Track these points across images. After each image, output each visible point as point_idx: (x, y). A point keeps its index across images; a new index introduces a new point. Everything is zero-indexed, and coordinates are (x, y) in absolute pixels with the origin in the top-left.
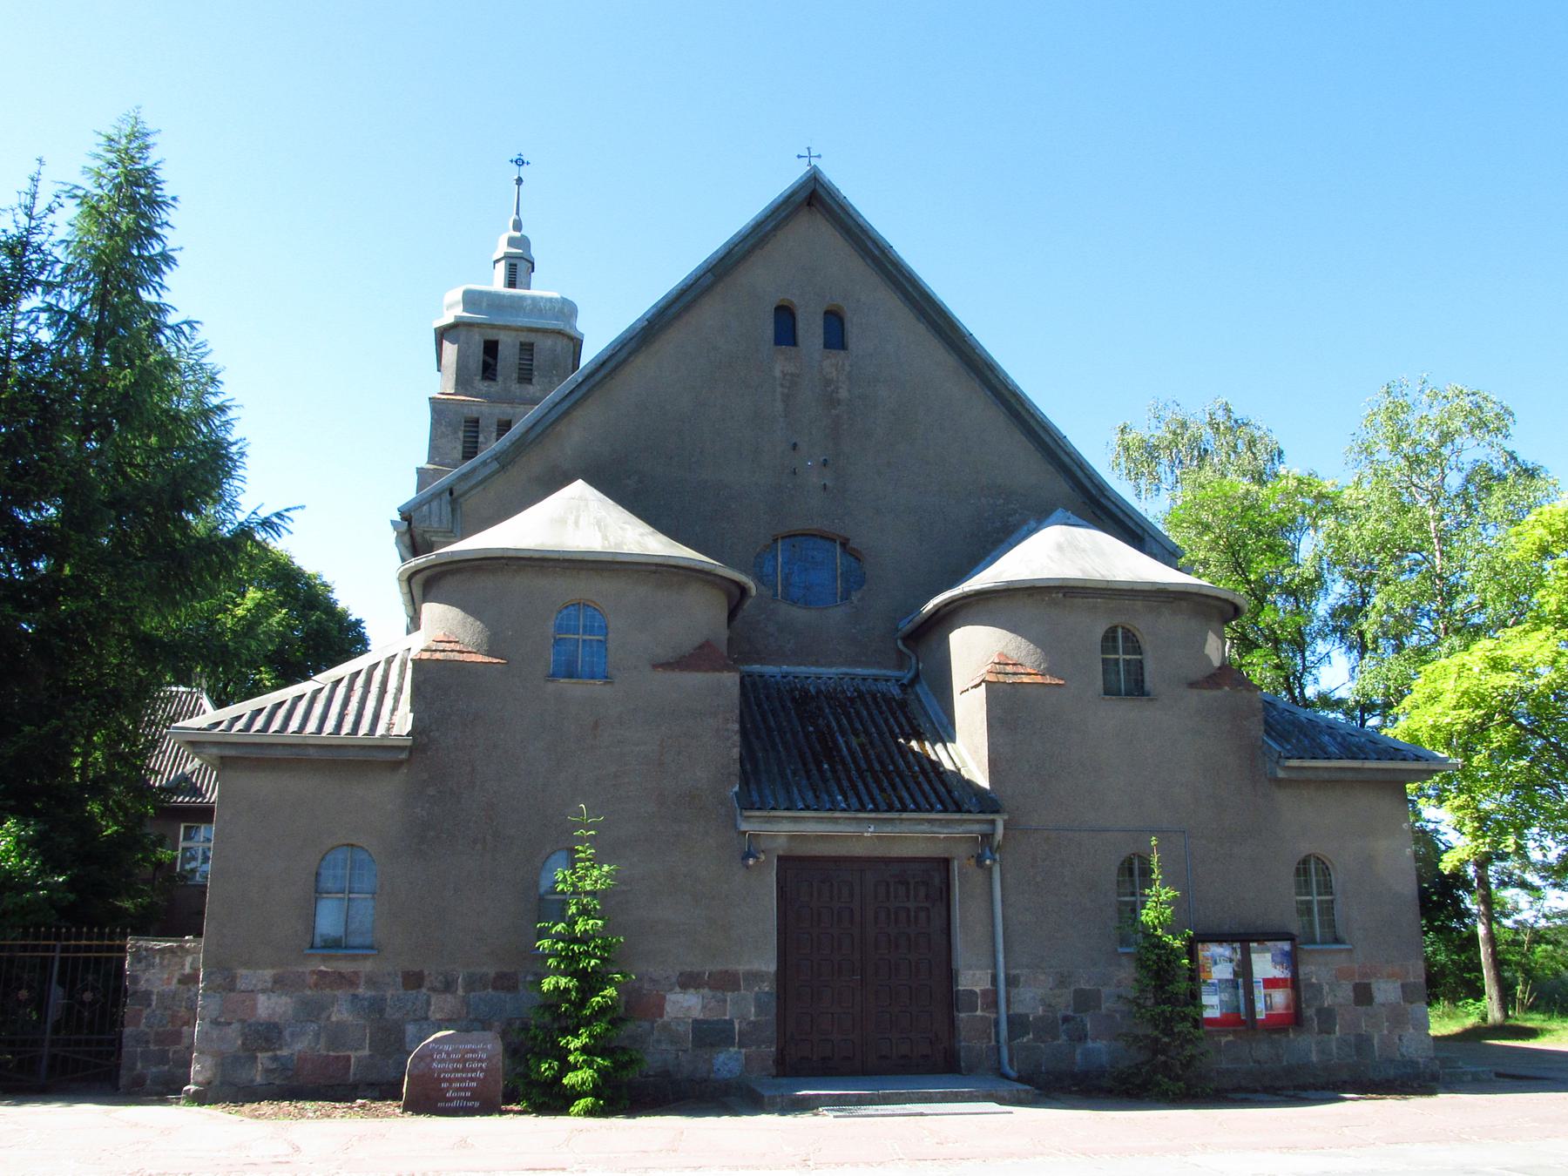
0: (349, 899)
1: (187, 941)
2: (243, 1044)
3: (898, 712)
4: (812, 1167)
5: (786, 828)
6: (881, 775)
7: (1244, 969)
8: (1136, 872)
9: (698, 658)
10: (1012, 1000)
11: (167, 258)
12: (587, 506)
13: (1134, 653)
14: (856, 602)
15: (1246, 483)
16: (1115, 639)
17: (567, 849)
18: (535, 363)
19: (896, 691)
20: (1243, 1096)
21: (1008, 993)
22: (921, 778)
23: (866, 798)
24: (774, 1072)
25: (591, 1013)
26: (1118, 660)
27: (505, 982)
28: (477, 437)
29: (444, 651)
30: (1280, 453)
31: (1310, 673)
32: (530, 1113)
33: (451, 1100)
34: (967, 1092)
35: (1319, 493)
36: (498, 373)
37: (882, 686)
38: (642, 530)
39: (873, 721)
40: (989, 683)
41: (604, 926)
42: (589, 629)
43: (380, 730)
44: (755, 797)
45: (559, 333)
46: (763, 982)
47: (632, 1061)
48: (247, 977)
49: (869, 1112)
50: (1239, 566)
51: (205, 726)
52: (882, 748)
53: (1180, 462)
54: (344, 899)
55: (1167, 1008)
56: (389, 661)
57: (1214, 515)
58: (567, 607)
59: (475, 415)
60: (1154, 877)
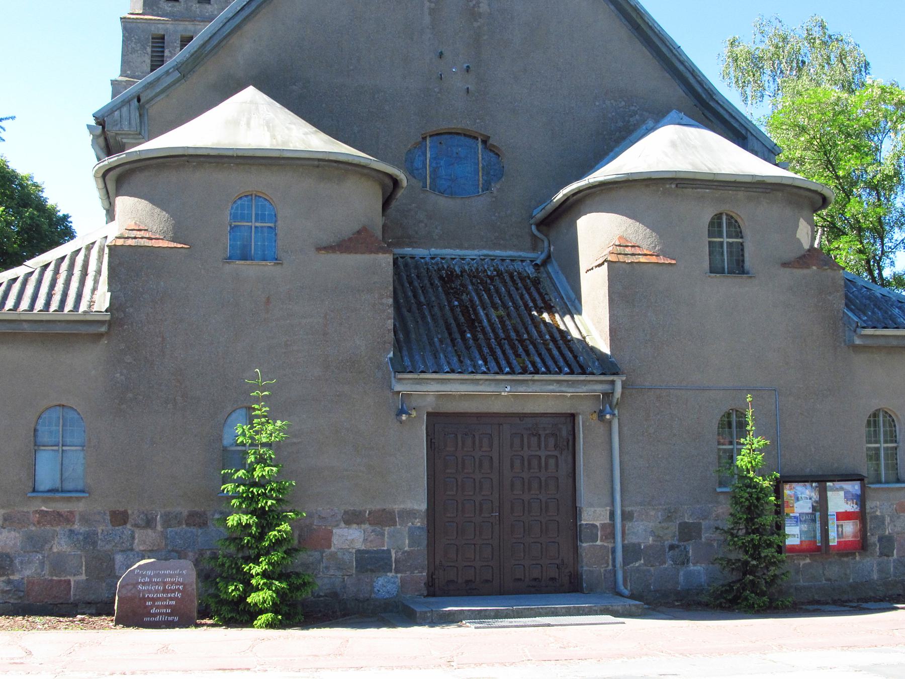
0: (63, 450)
3: (532, 288)
4: (455, 667)
6: (516, 342)
7: (821, 506)
8: (734, 424)
10: (627, 532)
12: (257, 109)
13: (737, 237)
14: (495, 192)
15: (837, 91)
16: (720, 225)
17: (246, 408)
19: (530, 270)
20: (816, 607)
21: (623, 526)
22: (551, 346)
23: (503, 363)
24: (425, 593)
25: (269, 545)
26: (722, 243)
27: (197, 519)
28: (163, 52)
29: (135, 238)
30: (867, 65)
31: (887, 257)
32: (221, 626)
33: (155, 615)
34: (587, 607)
35: (899, 101)
37: (518, 266)
38: (306, 130)
39: (510, 296)
40: (610, 263)
41: (279, 472)
42: (260, 217)
43: (83, 307)
44: (407, 362)
46: (416, 518)
47: (304, 584)
49: (503, 624)
50: (830, 165)
52: (518, 320)
53: (782, 72)
54: (58, 450)
55: (756, 537)
56: (89, 248)
57: (809, 118)
58: (240, 198)
60: (748, 428)
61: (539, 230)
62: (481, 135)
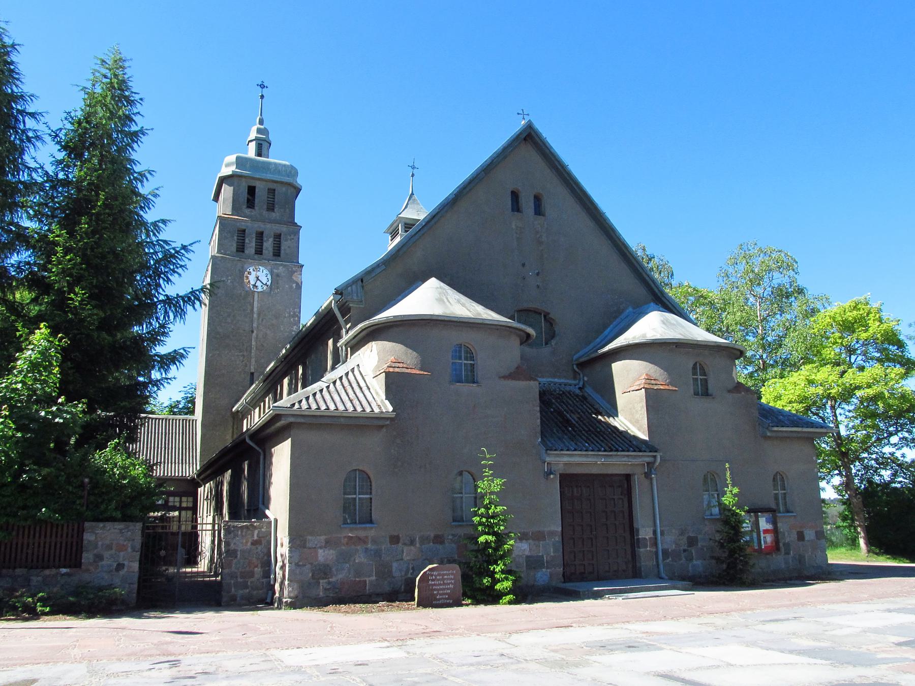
1: (254, 522)
2: (312, 575)
5: (566, 459)
9: (516, 374)
11: (142, 132)
18: (276, 200)
28: (244, 240)
30: (672, 275)
33: (439, 600)
36: (256, 205)
40: (646, 389)
45: (289, 185)
46: (556, 536)
48: (312, 541)
51: (289, 406)
59: (244, 228)
61: (578, 368)
62: (544, 312)
